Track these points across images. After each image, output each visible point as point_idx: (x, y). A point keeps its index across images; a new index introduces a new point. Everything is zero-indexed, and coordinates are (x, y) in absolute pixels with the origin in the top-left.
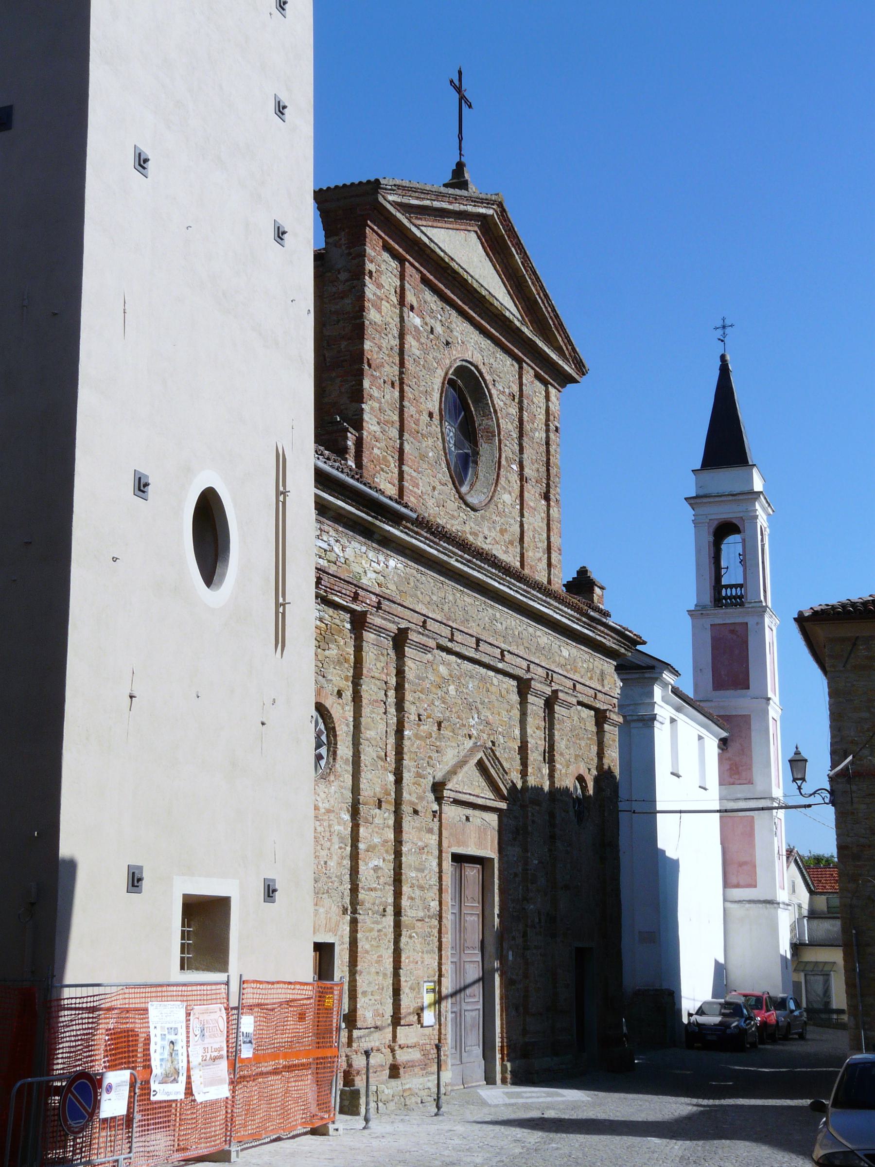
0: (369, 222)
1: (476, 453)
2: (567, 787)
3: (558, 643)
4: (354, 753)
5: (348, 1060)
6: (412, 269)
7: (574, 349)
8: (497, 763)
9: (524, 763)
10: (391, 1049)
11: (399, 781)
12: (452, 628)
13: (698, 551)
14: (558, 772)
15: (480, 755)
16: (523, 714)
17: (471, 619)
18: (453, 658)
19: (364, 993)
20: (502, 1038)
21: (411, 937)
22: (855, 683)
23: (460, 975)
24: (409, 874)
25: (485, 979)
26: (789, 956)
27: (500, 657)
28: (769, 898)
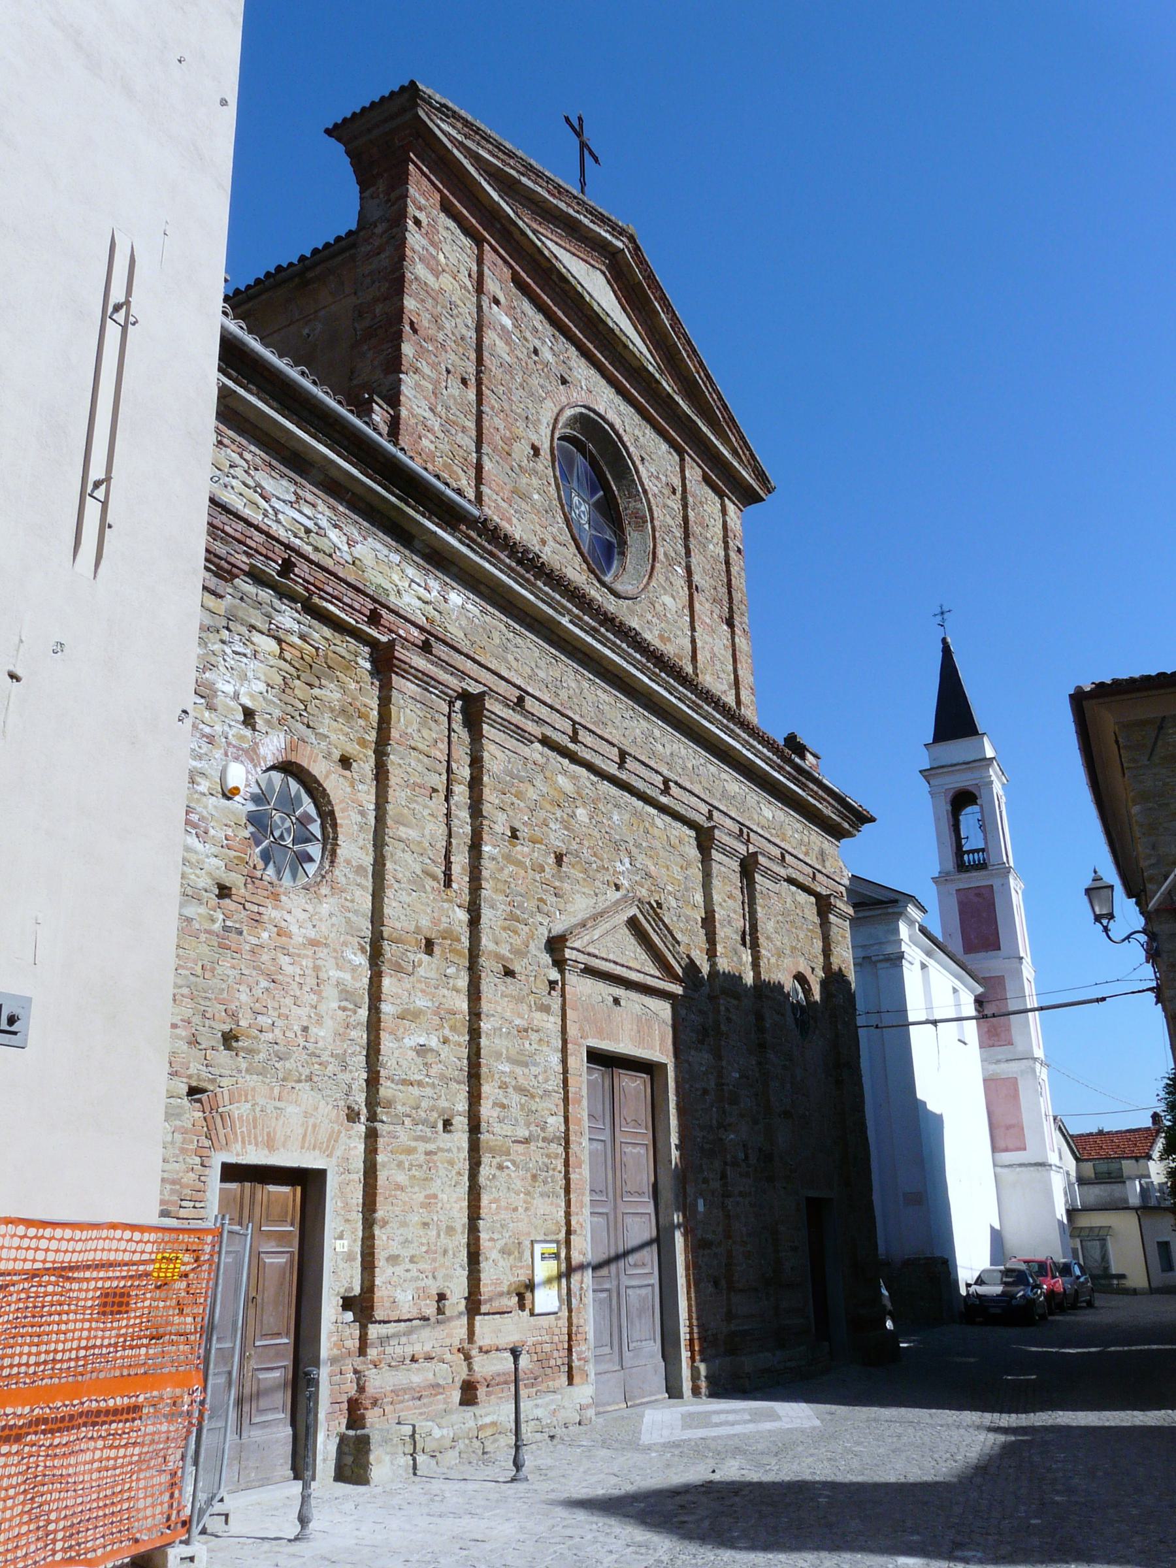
0: (412, 155)
1: (623, 543)
2: (779, 982)
3: (757, 798)
4: (375, 860)
5: (358, 1379)
6: (495, 256)
7: (752, 455)
8: (662, 926)
9: (711, 939)
10: (464, 1354)
11: (474, 922)
12: (574, 723)
13: (937, 819)
14: (765, 960)
15: (634, 911)
16: (707, 875)
17: (609, 723)
18: (583, 771)
19: (393, 1259)
20: (691, 1326)
21: (500, 1167)
22: (1168, 780)
23: (616, 1235)
24: (494, 1067)
25: (661, 1242)
26: (1065, 1221)
27: (662, 787)
28: (1040, 1161)
